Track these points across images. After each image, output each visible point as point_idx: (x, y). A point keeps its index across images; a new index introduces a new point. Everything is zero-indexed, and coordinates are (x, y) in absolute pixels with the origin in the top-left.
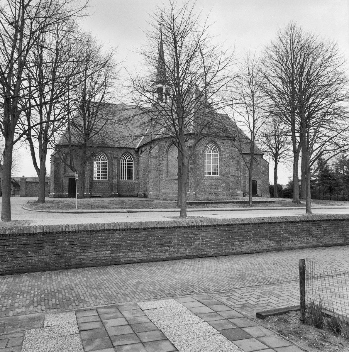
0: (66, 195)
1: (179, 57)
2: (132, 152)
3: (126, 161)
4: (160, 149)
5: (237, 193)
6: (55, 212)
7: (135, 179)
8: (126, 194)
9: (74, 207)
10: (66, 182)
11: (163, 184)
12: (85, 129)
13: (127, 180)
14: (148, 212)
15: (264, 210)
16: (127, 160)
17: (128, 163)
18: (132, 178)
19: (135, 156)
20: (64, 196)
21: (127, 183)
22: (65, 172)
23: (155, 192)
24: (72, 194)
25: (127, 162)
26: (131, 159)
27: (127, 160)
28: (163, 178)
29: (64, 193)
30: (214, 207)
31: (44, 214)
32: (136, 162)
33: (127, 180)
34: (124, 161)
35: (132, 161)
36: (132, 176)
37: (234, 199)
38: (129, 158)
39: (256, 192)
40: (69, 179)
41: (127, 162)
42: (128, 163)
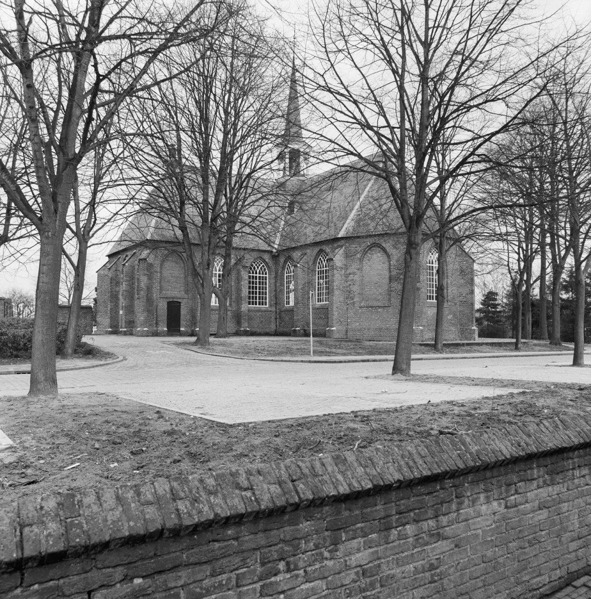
0: (164, 331)
1: (488, 135)
2: (266, 257)
3: (256, 273)
4: (347, 256)
5: (471, 330)
6: (297, 361)
7: (271, 306)
8: (258, 331)
9: (308, 354)
10: (163, 306)
11: (355, 314)
12: (201, 217)
13: (258, 306)
14: (422, 359)
15: (549, 355)
16: (218, 269)
17: (260, 277)
18: (266, 303)
19: (271, 263)
20: (160, 333)
21: (259, 311)
22: (161, 289)
23: (340, 327)
24: (173, 327)
25: (258, 275)
26: (265, 270)
27: (218, 269)
28: (354, 303)
29: (160, 329)
30: (467, 351)
31: (267, 365)
32: (273, 276)
33: (258, 306)
34: (253, 273)
35: (266, 274)
36: (266, 299)
37: (467, 339)
38: (261, 269)
39: (179, 327)
40: (169, 303)
41: (258, 275)
42: (260, 277)
